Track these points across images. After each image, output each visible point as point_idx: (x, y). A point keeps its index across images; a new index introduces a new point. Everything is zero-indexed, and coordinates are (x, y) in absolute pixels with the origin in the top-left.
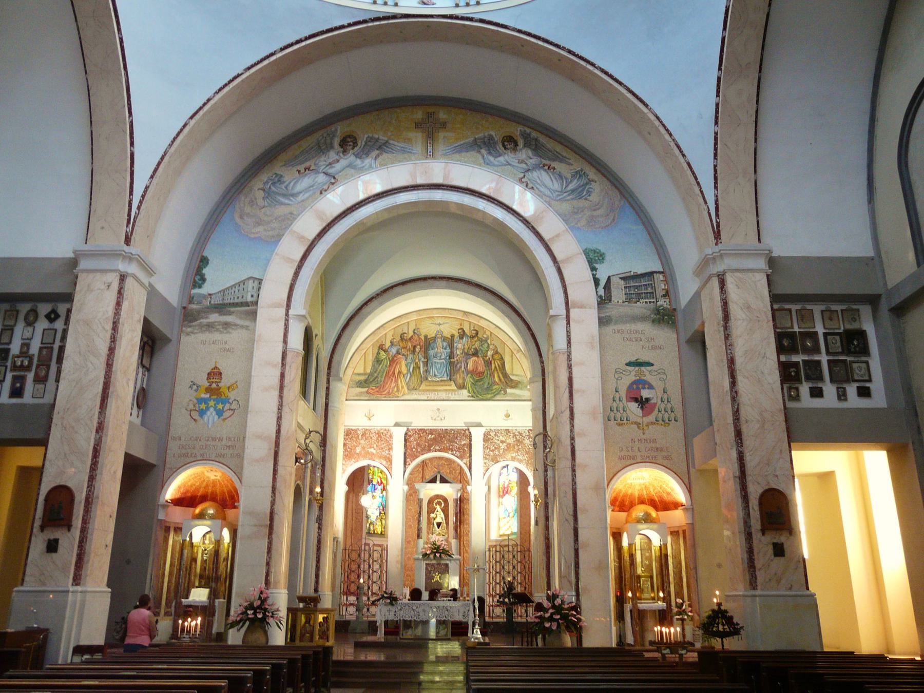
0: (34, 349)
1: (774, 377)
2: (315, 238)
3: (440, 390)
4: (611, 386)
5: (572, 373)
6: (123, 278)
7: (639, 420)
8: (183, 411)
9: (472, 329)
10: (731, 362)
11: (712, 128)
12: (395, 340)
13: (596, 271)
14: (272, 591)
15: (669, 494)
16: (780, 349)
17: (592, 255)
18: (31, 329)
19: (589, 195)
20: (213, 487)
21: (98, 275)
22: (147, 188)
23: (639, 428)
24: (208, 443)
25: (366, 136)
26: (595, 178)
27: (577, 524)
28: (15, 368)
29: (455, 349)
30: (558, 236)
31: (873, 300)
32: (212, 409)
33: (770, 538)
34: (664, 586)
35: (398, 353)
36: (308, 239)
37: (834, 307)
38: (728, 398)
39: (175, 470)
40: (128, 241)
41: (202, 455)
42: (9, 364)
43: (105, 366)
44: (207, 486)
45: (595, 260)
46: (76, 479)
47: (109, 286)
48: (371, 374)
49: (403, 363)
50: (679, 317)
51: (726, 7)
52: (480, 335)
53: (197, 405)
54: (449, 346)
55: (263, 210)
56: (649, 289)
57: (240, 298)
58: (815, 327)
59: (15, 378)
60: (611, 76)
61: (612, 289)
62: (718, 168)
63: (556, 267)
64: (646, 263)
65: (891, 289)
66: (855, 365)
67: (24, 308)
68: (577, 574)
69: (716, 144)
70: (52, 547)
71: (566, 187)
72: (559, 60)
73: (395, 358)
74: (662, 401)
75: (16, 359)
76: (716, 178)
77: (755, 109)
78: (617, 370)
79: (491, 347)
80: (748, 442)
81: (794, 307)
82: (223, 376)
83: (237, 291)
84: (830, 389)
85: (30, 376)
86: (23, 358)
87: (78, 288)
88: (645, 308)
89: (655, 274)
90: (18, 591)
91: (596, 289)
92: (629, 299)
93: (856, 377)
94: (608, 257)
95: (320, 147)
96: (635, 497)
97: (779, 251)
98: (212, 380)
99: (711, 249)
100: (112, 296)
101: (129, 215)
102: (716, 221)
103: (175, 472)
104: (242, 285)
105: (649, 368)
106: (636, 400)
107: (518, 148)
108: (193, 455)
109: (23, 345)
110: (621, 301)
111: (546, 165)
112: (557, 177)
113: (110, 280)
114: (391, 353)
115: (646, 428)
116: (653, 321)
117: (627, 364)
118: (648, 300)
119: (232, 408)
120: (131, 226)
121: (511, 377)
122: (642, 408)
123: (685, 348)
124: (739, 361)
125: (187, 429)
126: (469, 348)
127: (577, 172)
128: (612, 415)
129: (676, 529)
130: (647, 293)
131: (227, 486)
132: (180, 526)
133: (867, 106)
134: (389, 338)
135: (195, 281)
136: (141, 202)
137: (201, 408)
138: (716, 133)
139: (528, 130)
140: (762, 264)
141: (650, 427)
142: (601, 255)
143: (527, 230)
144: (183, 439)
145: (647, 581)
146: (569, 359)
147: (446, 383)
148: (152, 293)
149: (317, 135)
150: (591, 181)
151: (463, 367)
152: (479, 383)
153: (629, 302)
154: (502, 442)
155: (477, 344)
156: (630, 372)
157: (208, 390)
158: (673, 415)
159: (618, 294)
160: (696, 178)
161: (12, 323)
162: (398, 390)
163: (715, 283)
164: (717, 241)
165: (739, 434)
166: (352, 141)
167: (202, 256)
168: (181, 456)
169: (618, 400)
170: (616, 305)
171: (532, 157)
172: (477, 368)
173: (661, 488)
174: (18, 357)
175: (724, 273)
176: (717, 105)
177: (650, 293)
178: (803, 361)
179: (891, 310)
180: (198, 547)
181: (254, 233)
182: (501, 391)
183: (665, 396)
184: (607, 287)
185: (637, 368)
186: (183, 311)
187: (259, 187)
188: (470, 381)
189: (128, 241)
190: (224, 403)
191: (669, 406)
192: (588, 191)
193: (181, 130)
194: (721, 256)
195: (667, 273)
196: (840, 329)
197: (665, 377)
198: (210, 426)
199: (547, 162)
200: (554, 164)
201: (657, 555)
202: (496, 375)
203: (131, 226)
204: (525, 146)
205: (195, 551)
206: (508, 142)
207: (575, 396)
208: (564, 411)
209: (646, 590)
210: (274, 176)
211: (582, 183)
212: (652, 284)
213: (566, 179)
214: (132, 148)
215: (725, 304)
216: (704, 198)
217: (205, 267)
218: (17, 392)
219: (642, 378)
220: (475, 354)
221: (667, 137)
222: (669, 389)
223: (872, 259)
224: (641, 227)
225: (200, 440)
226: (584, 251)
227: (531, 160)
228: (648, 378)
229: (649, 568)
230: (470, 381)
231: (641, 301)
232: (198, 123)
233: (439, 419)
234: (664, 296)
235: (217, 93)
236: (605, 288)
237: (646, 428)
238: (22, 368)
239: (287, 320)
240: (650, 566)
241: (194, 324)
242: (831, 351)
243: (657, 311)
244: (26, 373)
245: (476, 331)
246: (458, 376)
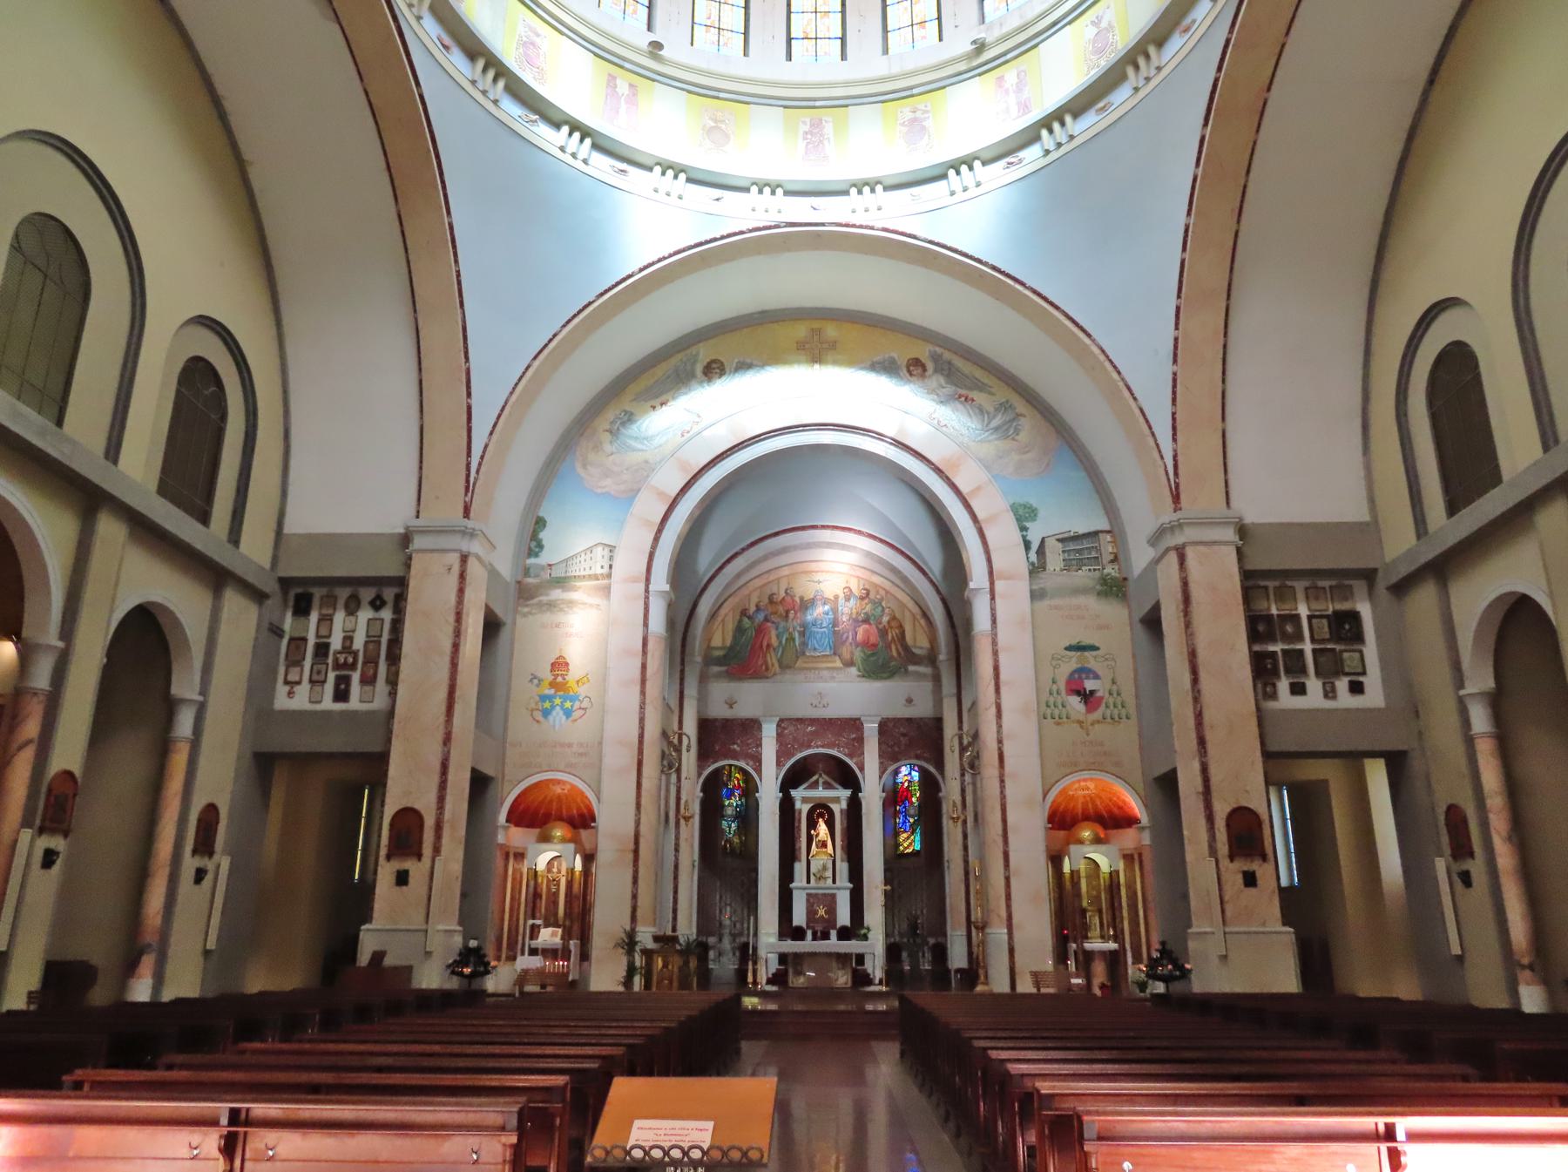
0: (359, 643)
2: (678, 494)
5: (998, 661)
6: (464, 559)
10: (1193, 655)
11: (1169, 368)
12: (761, 604)
13: (1026, 531)
14: (994, 931)
15: (1120, 808)
16: (1254, 636)
17: (1021, 512)
18: (352, 618)
19: (1017, 434)
21: (436, 555)
23: (1082, 727)
25: (736, 360)
27: (1007, 847)
28: (337, 666)
30: (978, 489)
31: (1369, 576)
32: (558, 708)
33: (1241, 865)
35: (766, 620)
37: (1321, 583)
38: (1190, 699)
40: (467, 512)
42: (330, 660)
43: (450, 666)
46: (425, 804)
47: (450, 569)
48: (731, 648)
50: (1131, 588)
51: (1186, 225)
52: (872, 596)
55: (611, 458)
57: (587, 569)
58: (1296, 609)
59: (339, 680)
62: (1177, 416)
63: (977, 528)
64: (1088, 520)
65: (1394, 561)
66: (1346, 655)
68: (1009, 906)
69: (1174, 386)
70: (402, 878)
71: (987, 425)
74: (1111, 694)
75: (338, 655)
76: (1174, 428)
77: (1222, 343)
78: (1055, 656)
79: (887, 611)
81: (1271, 584)
83: (582, 561)
84: (1314, 685)
85: (356, 677)
86: (347, 655)
87: (413, 571)
90: (368, 930)
91: (1027, 554)
92: (1068, 566)
93: (1347, 670)
94: (1042, 513)
95: (678, 375)
96: (1077, 814)
97: (1250, 518)
98: (557, 672)
99: (1168, 516)
101: (468, 481)
102: (1175, 482)
103: (517, 785)
105: (1094, 653)
106: (1078, 693)
110: (1058, 569)
111: (963, 396)
114: (757, 620)
115: (1090, 728)
116: (1099, 594)
117: (1066, 649)
118: (1092, 568)
119: (582, 706)
120: (470, 494)
121: (914, 650)
122: (1086, 703)
123: (1139, 628)
126: (857, 613)
127: (1001, 404)
128: (1049, 712)
129: (1129, 852)
132: (520, 851)
133: (1362, 334)
134: (754, 600)
136: (480, 464)
139: (939, 350)
140: (1230, 534)
141: (1096, 726)
142: (1033, 511)
143: (940, 480)
145: (1094, 916)
146: (994, 643)
149: (674, 361)
150: (1019, 415)
151: (851, 638)
153: (1068, 570)
154: (904, 735)
157: (553, 685)
158: (1124, 712)
159: (1055, 561)
160: (1150, 428)
161: (330, 611)
162: (767, 669)
163: (1173, 558)
164: (1176, 506)
165: (1202, 742)
166: (718, 368)
167: (538, 517)
169: (1055, 693)
171: (945, 385)
172: (868, 638)
173: (1110, 801)
174: (339, 653)
175: (1184, 546)
176: (1176, 339)
177: (1094, 557)
178: (1282, 650)
179: (1388, 589)
180: (543, 877)
182: (900, 668)
183: (1115, 688)
184: (1041, 551)
185: (1079, 653)
186: (518, 586)
189: (467, 512)
190: (572, 699)
192: (1016, 429)
194: (1180, 526)
195: (1116, 531)
196: (1326, 610)
197: (1113, 664)
199: (963, 392)
201: (1107, 884)
203: (470, 494)
204: (936, 371)
206: (914, 366)
207: (1003, 690)
209: (1093, 927)
210: (623, 414)
211: (1007, 419)
214: (469, 400)
215: (1185, 584)
216: (1160, 452)
217: (541, 531)
218: (341, 695)
219: (1086, 665)
221: (1115, 375)
223: (1367, 524)
224: (1084, 474)
226: (1011, 506)
227: (944, 390)
229: (1096, 900)
233: (821, 705)
234: (1112, 561)
236: (1037, 553)
238: (345, 666)
239: (647, 598)
240: (1098, 897)
242: (1316, 637)
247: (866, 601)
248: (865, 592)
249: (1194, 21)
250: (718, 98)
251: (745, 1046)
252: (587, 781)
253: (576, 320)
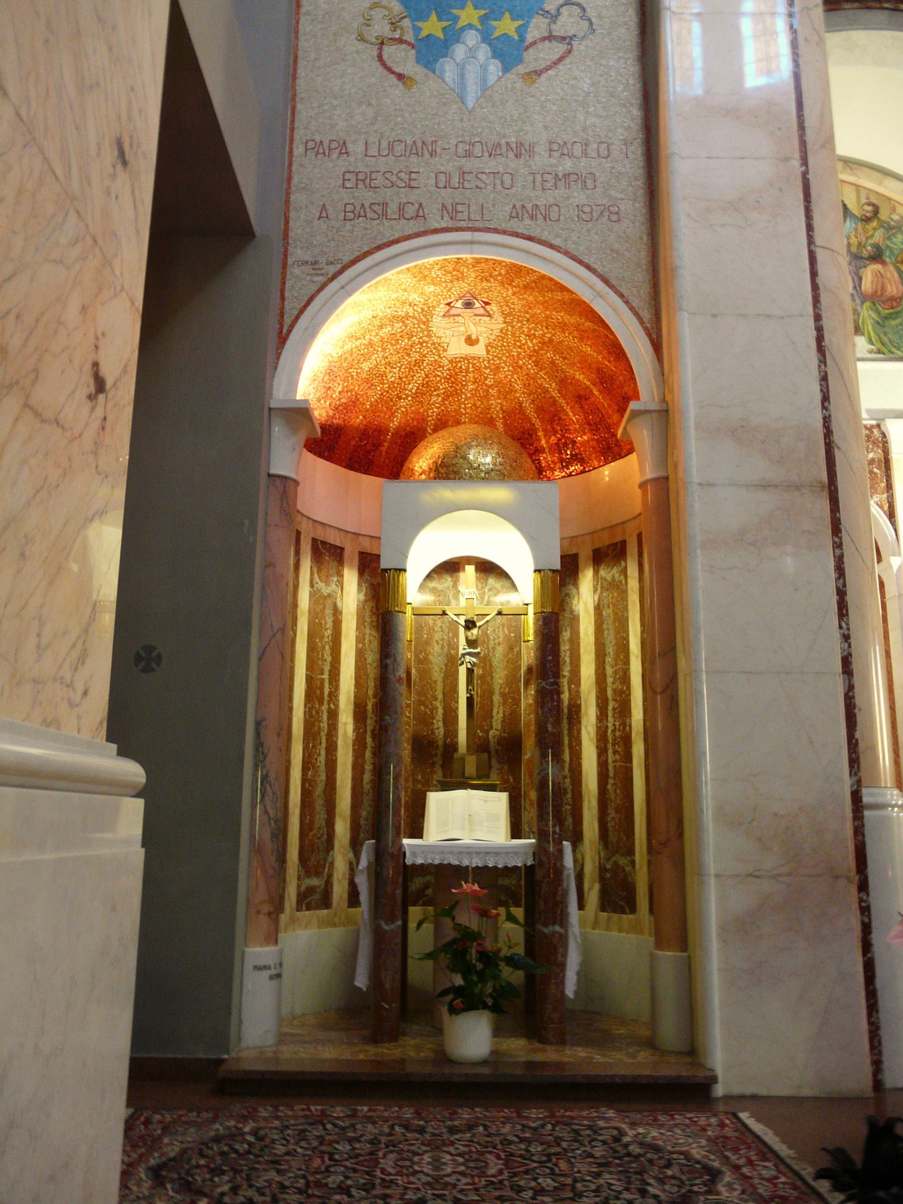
8: (350, 44)
9: (864, 201)
20: (447, 396)
24: (469, 165)
32: (472, 38)
39: (332, 270)
41: (453, 213)
44: (426, 388)
52: (884, 215)
53: (406, 23)
108: (410, 211)
125: (370, 113)
126: (860, 244)
131: (506, 391)
137: (424, 34)
144: (356, 148)
152: (893, 323)
155: (878, 236)
168: (355, 213)
188: (870, 316)
198: (470, 103)
220: (877, 256)
225: (433, 154)
230: (870, 316)
245: (873, 205)
247: (875, 224)
248: (869, 208)
251: (861, 1167)
252: (597, 267)
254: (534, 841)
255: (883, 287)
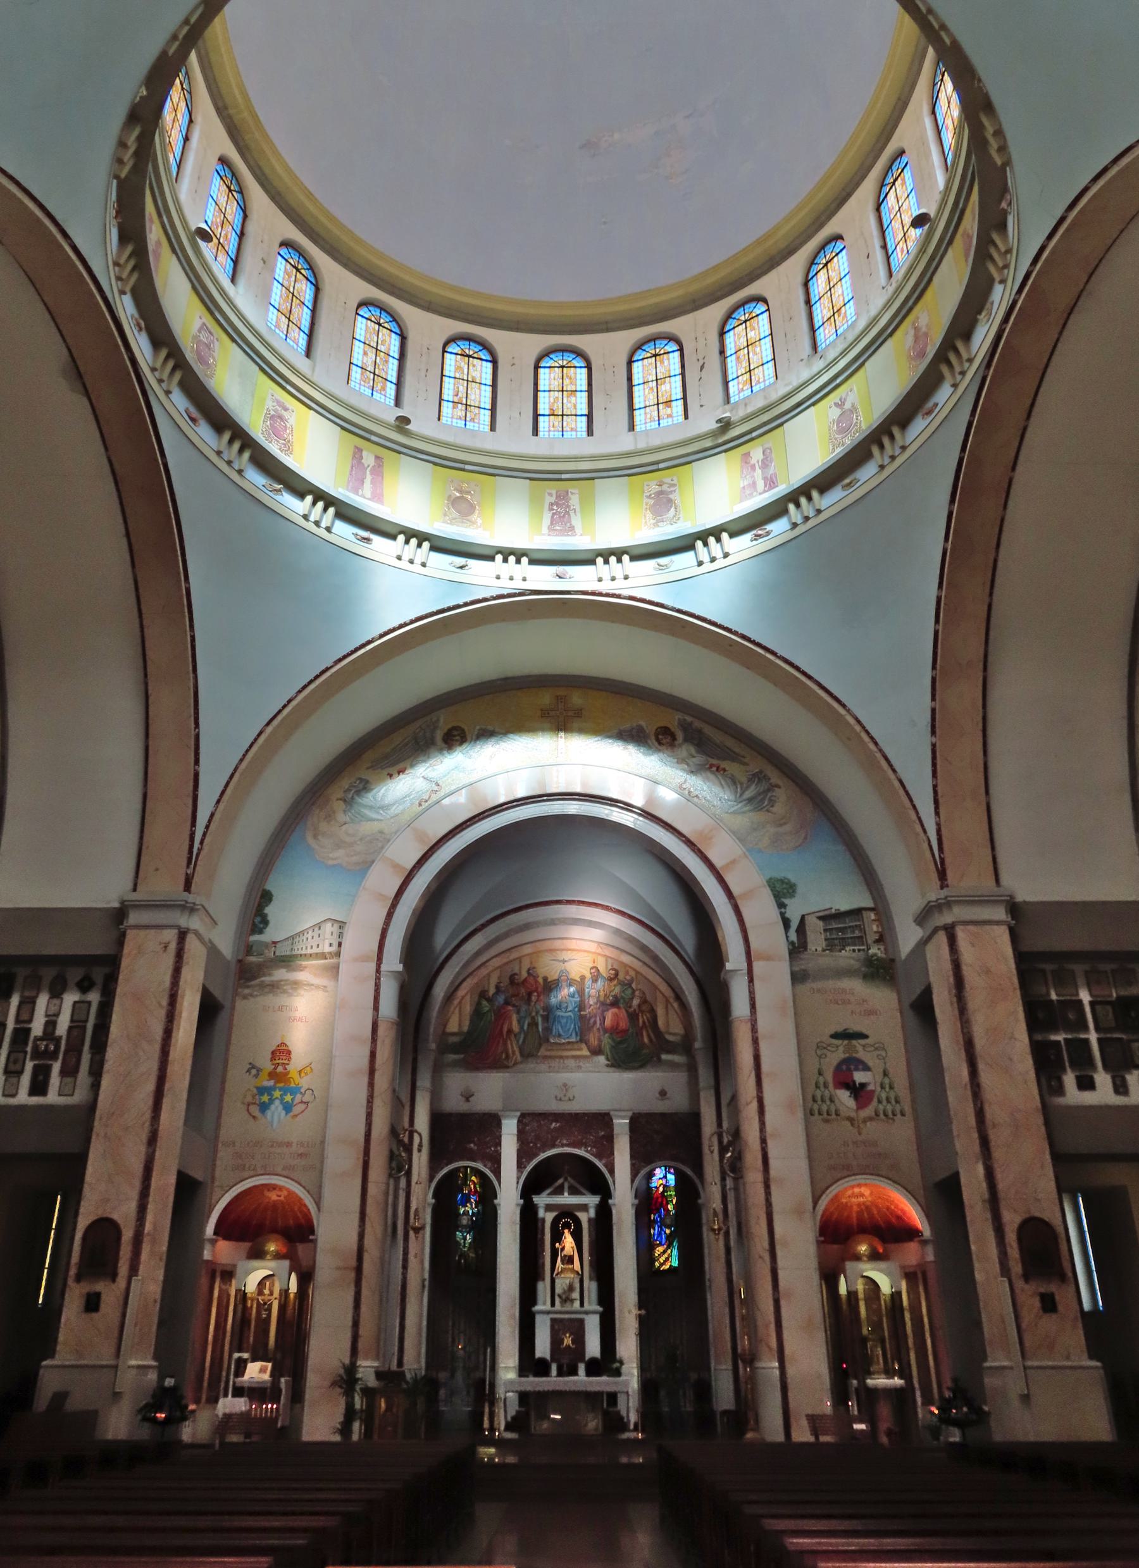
1: (1025, 1065)
3: (567, 1057)
4: (813, 1065)
6: (182, 935)
7: (853, 1114)
9: (610, 967)
11: (927, 739)
12: (502, 985)
17: (778, 887)
18: (56, 1001)
19: (772, 806)
22: (212, 815)
23: (852, 1125)
25: (478, 727)
26: (780, 783)
29: (586, 997)
30: (733, 862)
32: (277, 1102)
34: (900, 1352)
35: (507, 1003)
36: (404, 868)
40: (188, 887)
42: (29, 1049)
45: (784, 894)
46: (124, 1213)
47: (166, 947)
48: (469, 1033)
49: (514, 1017)
54: (578, 992)
55: (344, 828)
56: (857, 932)
60: (797, 668)
61: (808, 933)
62: (939, 789)
67: (49, 974)
69: (934, 758)
70: (92, 1303)
71: (741, 795)
72: (731, 645)
73: (503, 1011)
79: (637, 993)
80: (998, 1154)
82: (293, 1055)
83: (310, 938)
84: (1103, 1079)
85: (56, 1067)
88: (853, 958)
89: (864, 912)
90: (47, 1367)
91: (786, 934)
94: (800, 889)
97: (1025, 894)
100: (169, 960)
104: (316, 929)
105: (863, 1042)
107: (676, 743)
108: (253, 1167)
109: (47, 1024)
110: (820, 949)
112: (729, 781)
113: (166, 940)
114: (497, 1003)
118: (856, 948)
120: (192, 866)
123: (910, 1014)
124: (979, 1043)
126: (605, 995)
127: (754, 775)
129: (912, 1270)
130: (854, 937)
132: (229, 1269)
134: (494, 981)
135: (254, 924)
136: (204, 835)
138: (934, 746)
139: (689, 719)
140: (1000, 913)
145: (876, 1347)
146: (754, 1029)
147: (576, 1046)
148: (213, 951)
153: (831, 950)
156: (837, 1047)
157: (272, 1075)
159: (816, 940)
160: (911, 800)
161: (33, 994)
163: (942, 937)
165: (985, 1142)
166: (459, 735)
170: (813, 954)
176: (933, 710)
178: (1065, 1039)
181: (332, 859)
182: (652, 1057)
183: (887, 1081)
184: (801, 929)
187: (339, 796)
189: (188, 887)
191: (892, 1095)
192: (770, 800)
193: (256, 740)
195: (881, 909)
199: (715, 762)
200: (724, 764)
202: (645, 1034)
203: (192, 866)
205: (249, 1305)
206: (663, 734)
208: (751, 1102)
212: (860, 926)
213: (741, 784)
219: (854, 1055)
221: (872, 746)
222: (891, 1071)
227: (694, 760)
228: (861, 1054)
229: (877, 1326)
231: (848, 948)
232: (275, 730)
234: (877, 941)
235: (300, 692)
236: (797, 931)
237: (862, 1126)
239: (378, 979)
241: (253, 983)
243: (870, 961)
244: (51, 1062)
246: (591, 1035)
249: (936, 405)
250: (463, 470)
253: (312, 686)
254: (383, 1400)
255: (618, 1024)
